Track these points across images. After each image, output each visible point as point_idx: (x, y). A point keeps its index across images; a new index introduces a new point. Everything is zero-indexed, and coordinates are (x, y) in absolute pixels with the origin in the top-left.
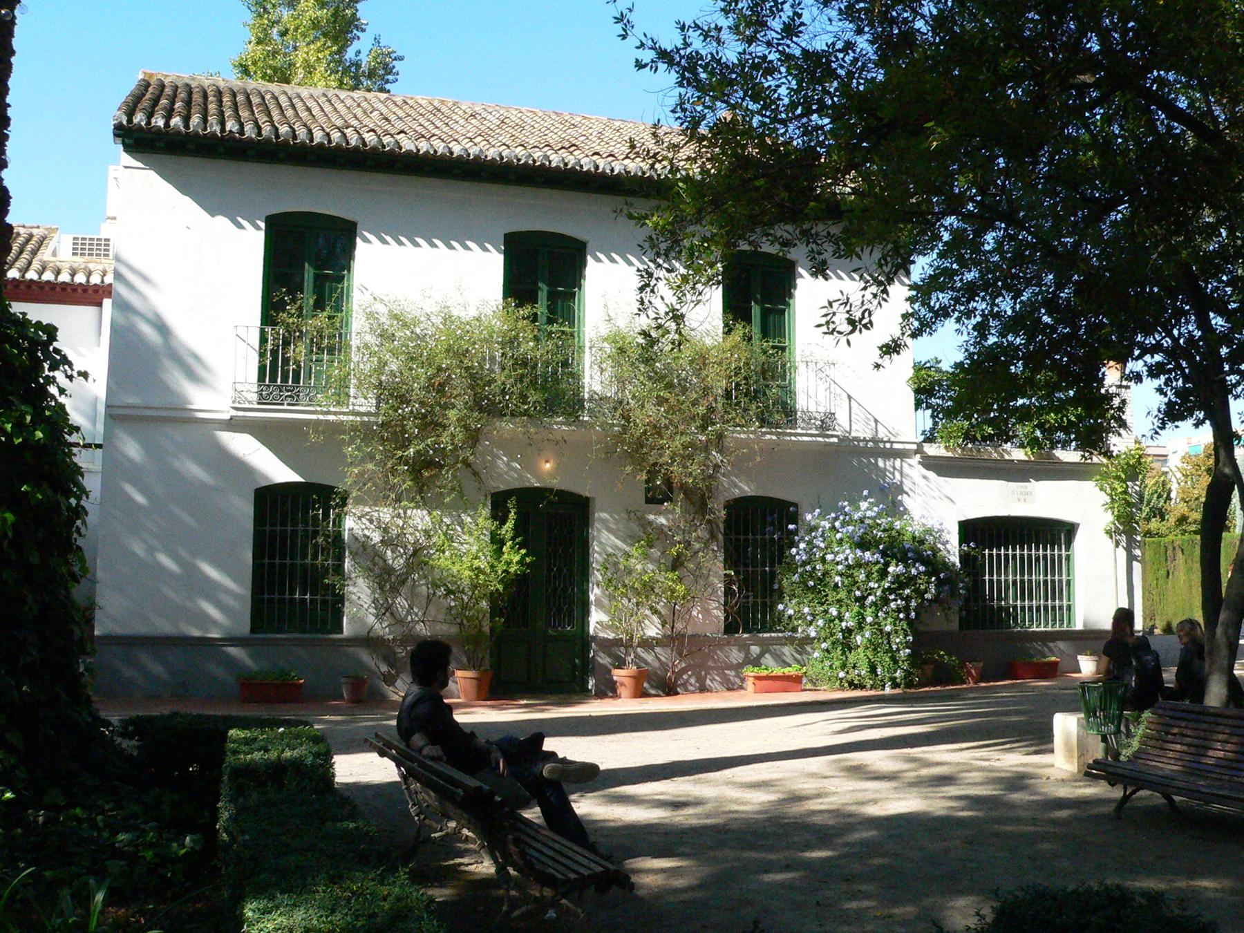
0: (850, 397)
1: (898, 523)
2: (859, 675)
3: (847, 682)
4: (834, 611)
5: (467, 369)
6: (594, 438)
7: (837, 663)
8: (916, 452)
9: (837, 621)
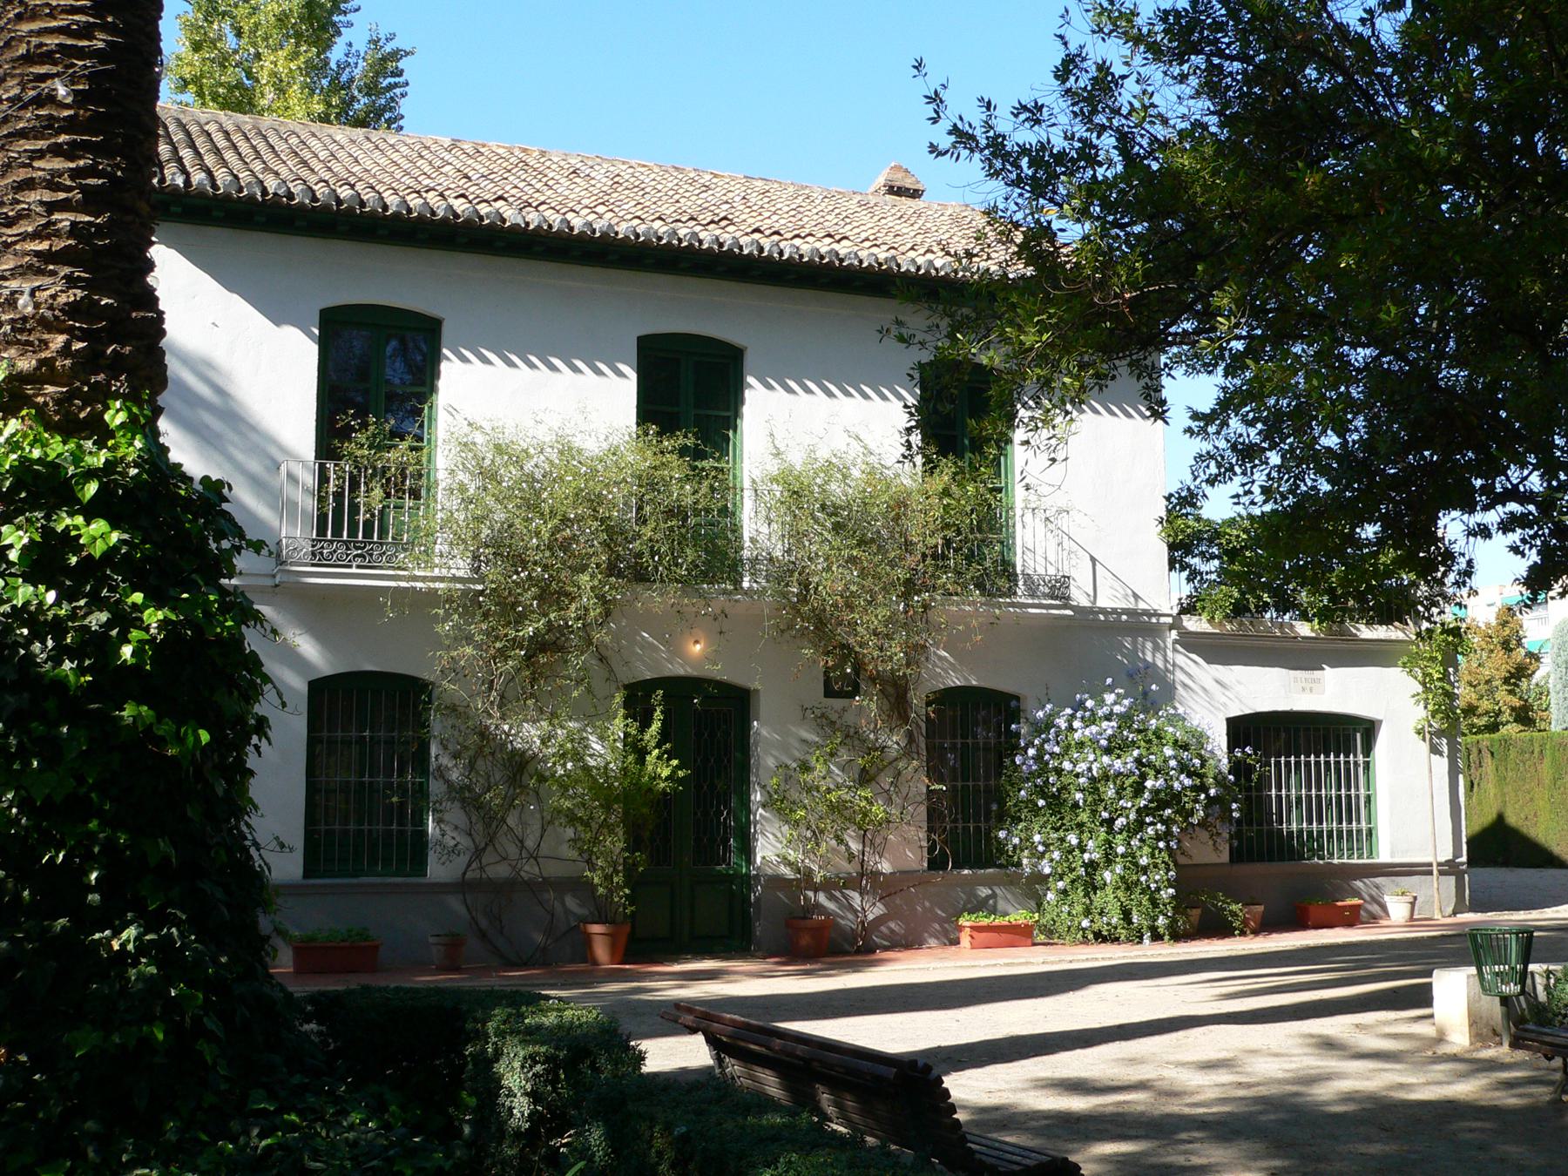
0: (1093, 560)
1: (1153, 721)
2: (1108, 924)
3: (1094, 933)
4: (1073, 839)
5: (603, 521)
6: (766, 611)
7: (1079, 908)
8: (1171, 627)
9: (1077, 852)
